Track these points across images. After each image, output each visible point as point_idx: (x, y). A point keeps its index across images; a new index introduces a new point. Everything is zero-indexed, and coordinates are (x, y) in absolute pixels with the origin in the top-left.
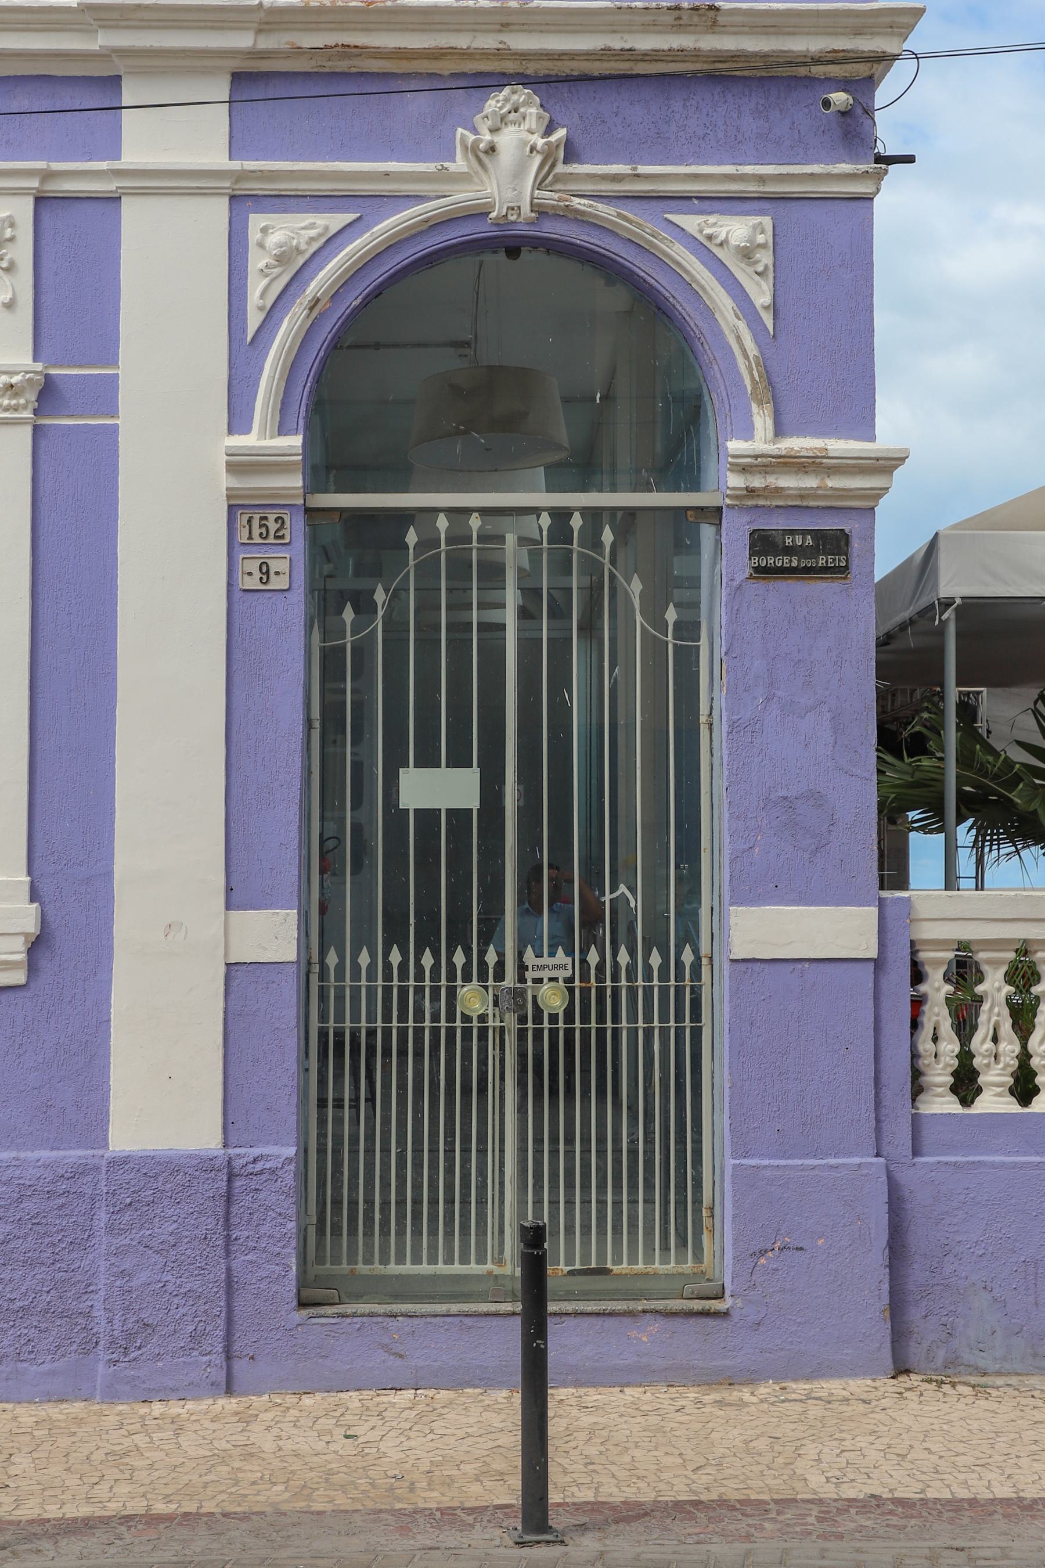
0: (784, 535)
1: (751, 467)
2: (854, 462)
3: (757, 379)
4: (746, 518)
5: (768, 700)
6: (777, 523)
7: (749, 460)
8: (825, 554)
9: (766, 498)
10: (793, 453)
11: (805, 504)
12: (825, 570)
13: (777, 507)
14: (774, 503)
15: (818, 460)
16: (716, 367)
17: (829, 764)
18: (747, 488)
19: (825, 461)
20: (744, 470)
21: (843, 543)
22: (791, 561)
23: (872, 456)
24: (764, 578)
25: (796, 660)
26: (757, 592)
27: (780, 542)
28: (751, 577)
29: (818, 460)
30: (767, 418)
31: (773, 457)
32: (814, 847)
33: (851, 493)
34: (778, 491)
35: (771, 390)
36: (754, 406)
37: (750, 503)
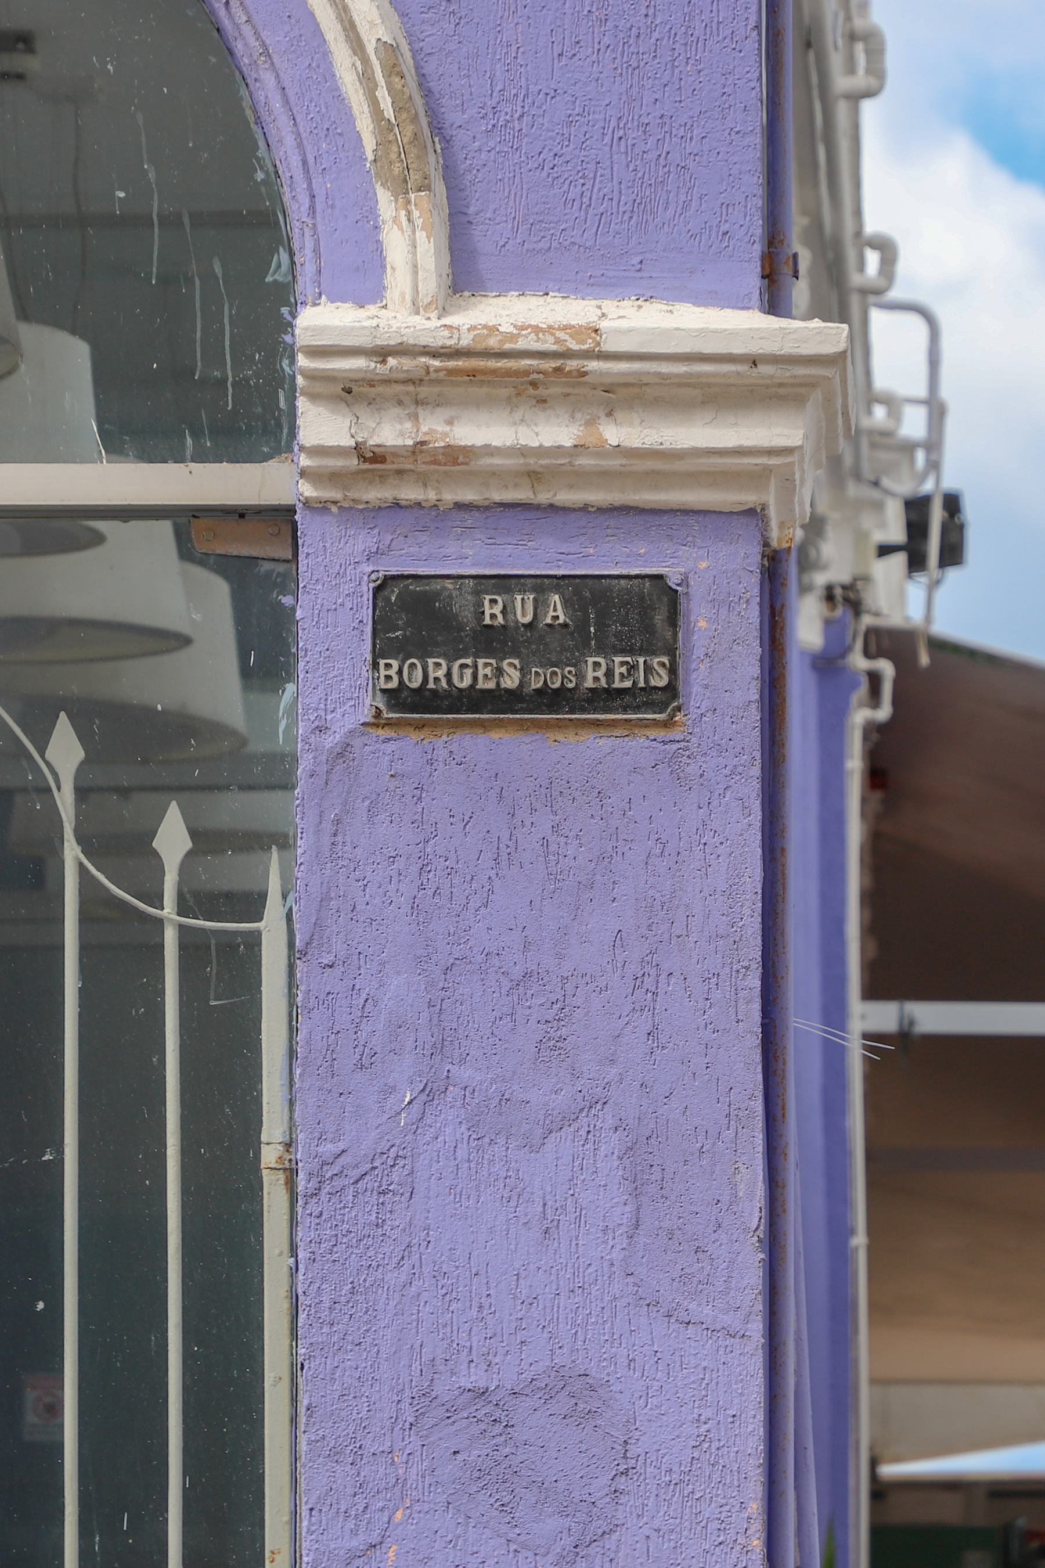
0: (477, 593)
1: (371, 384)
2: (681, 368)
3: (389, 113)
4: (362, 541)
5: (429, 1093)
6: (456, 557)
7: (359, 363)
8: (601, 650)
9: (424, 480)
10: (493, 342)
11: (543, 497)
12: (605, 698)
13: (460, 506)
14: (450, 496)
15: (572, 364)
16: (268, 78)
17: (616, 1288)
18: (358, 449)
19: (593, 365)
20: (349, 393)
21: (659, 618)
22: (499, 672)
23: (738, 349)
24: (420, 726)
25: (517, 972)
26: (398, 767)
27: (467, 615)
28: (378, 721)
29: (572, 364)
30: (421, 236)
31: (434, 354)
32: (568, 1541)
33: (679, 466)
34: (456, 457)
35: (434, 142)
36: (384, 199)
37: (375, 494)
